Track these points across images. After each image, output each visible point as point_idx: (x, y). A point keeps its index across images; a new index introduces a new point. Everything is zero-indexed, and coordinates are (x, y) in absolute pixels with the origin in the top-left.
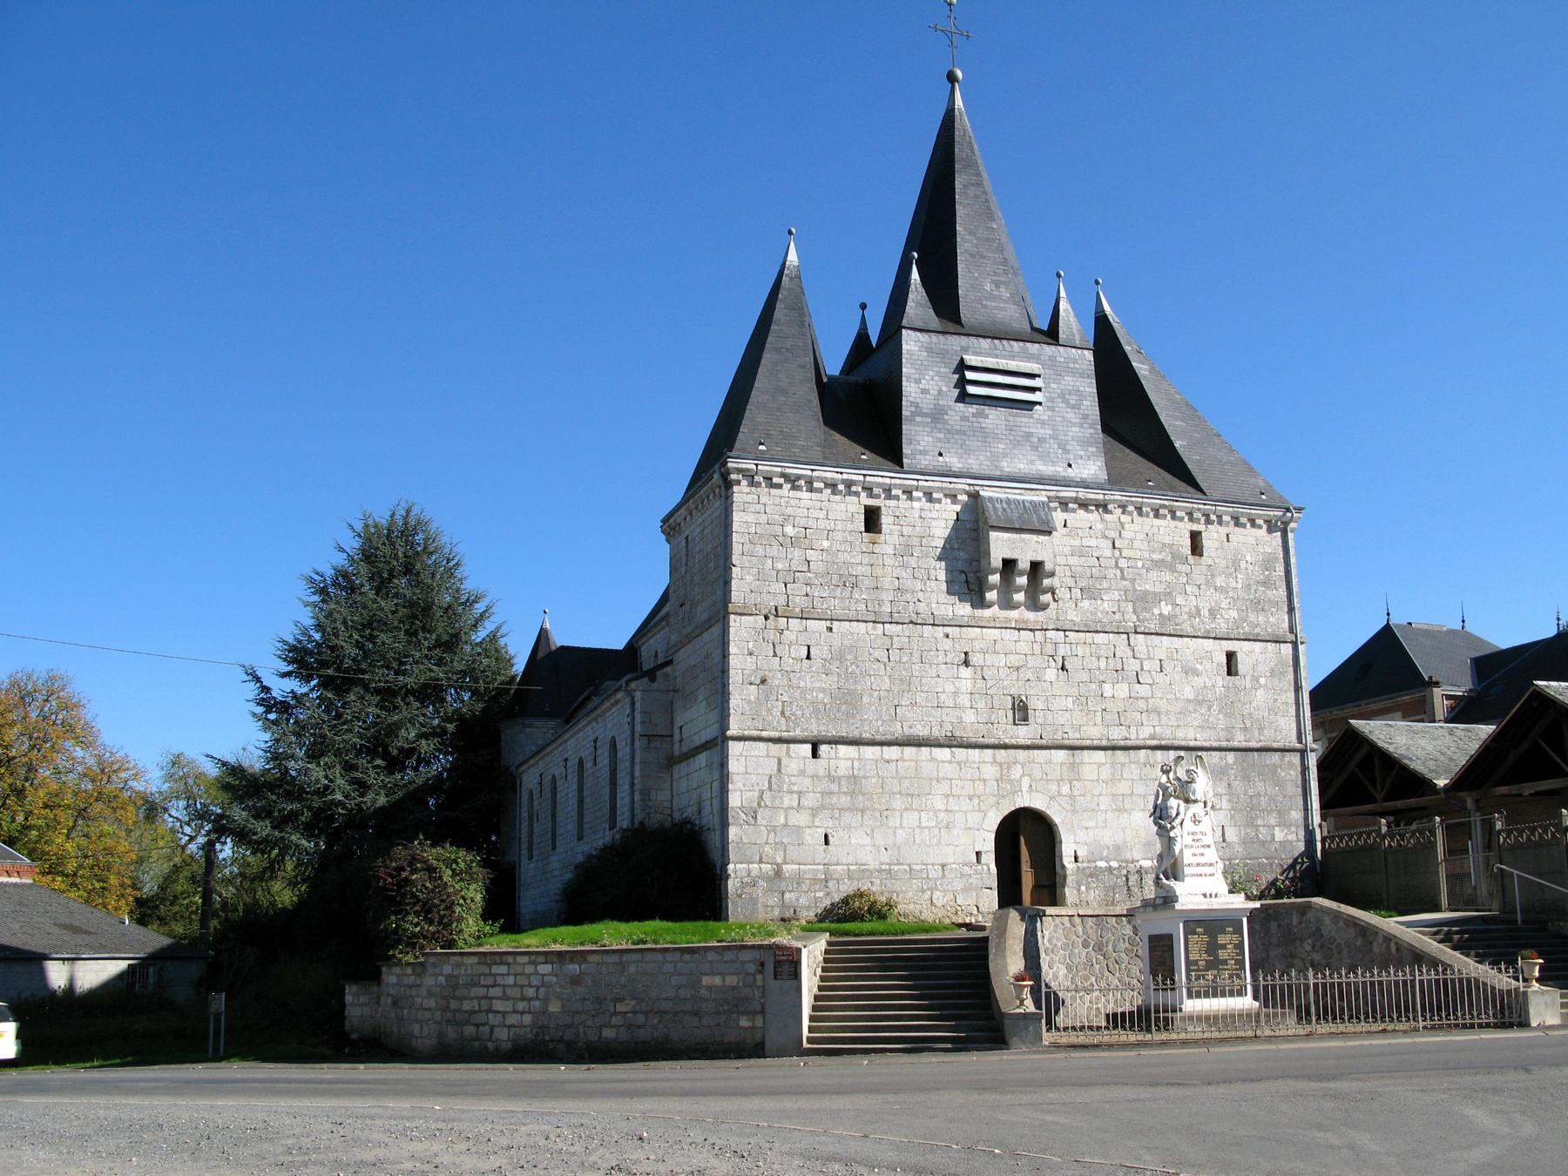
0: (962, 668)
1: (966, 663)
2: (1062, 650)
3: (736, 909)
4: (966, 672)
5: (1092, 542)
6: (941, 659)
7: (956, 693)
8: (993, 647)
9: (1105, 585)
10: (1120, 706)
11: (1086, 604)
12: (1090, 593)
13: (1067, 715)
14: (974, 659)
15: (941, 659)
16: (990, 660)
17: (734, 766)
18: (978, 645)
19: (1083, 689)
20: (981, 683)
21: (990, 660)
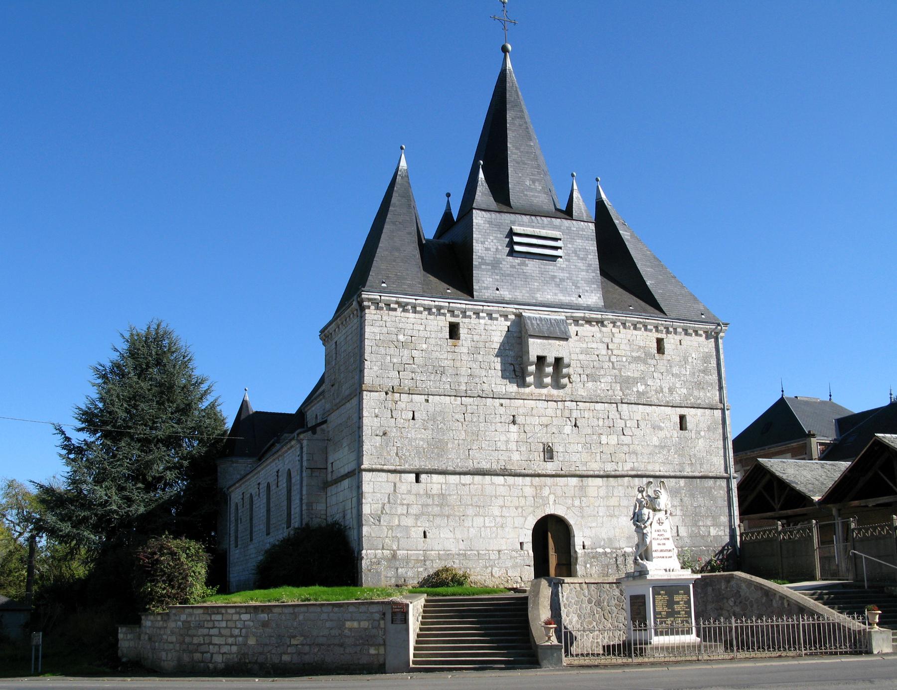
0: (512, 426)
1: (514, 422)
6: (498, 420)
7: (507, 442)
9: (602, 372)
10: (612, 450)
11: (590, 385)
13: (578, 455)
14: (519, 420)
16: (529, 420)
18: (521, 411)
20: (523, 435)
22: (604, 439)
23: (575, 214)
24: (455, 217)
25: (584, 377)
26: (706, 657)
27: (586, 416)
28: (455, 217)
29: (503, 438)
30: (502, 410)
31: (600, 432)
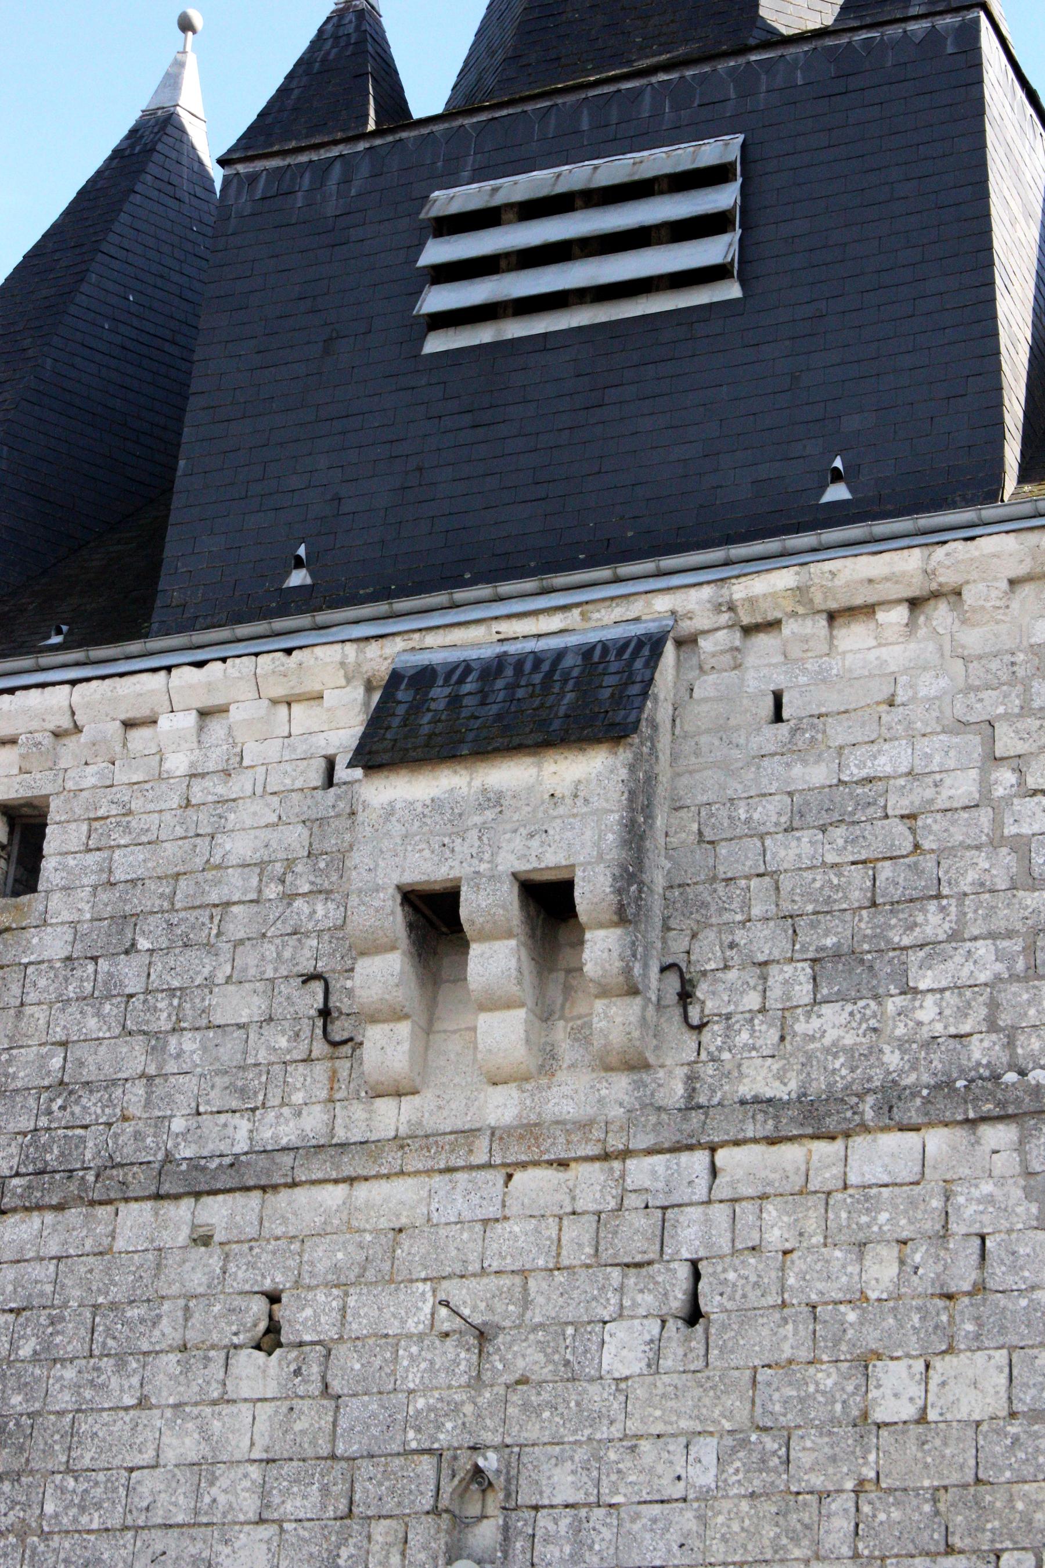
0: (250, 1361)
1: (270, 1338)
2: (689, 1236)
3: (730, 158)
4: (256, 1373)
5: (890, 760)
6: (168, 1331)
7: (202, 1470)
8: (384, 1260)
9: (933, 923)
10: (956, 1461)
11: (833, 1024)
12: (849, 969)
13: (686, 1520)
14: (301, 1319)
15: (168, 1331)
16: (367, 1311)
17: (498, 945)
18: (323, 1257)
19: (778, 1398)
20: (312, 1418)
21: (367, 1311)
22: (895, 1392)
23: (825, 616)
24: (427, 91)
25: (794, 981)
26: (994, 665)
27: (775, 1237)
28: (427, 91)
29: (182, 1445)
30: (197, 1271)
31: (871, 1339)
